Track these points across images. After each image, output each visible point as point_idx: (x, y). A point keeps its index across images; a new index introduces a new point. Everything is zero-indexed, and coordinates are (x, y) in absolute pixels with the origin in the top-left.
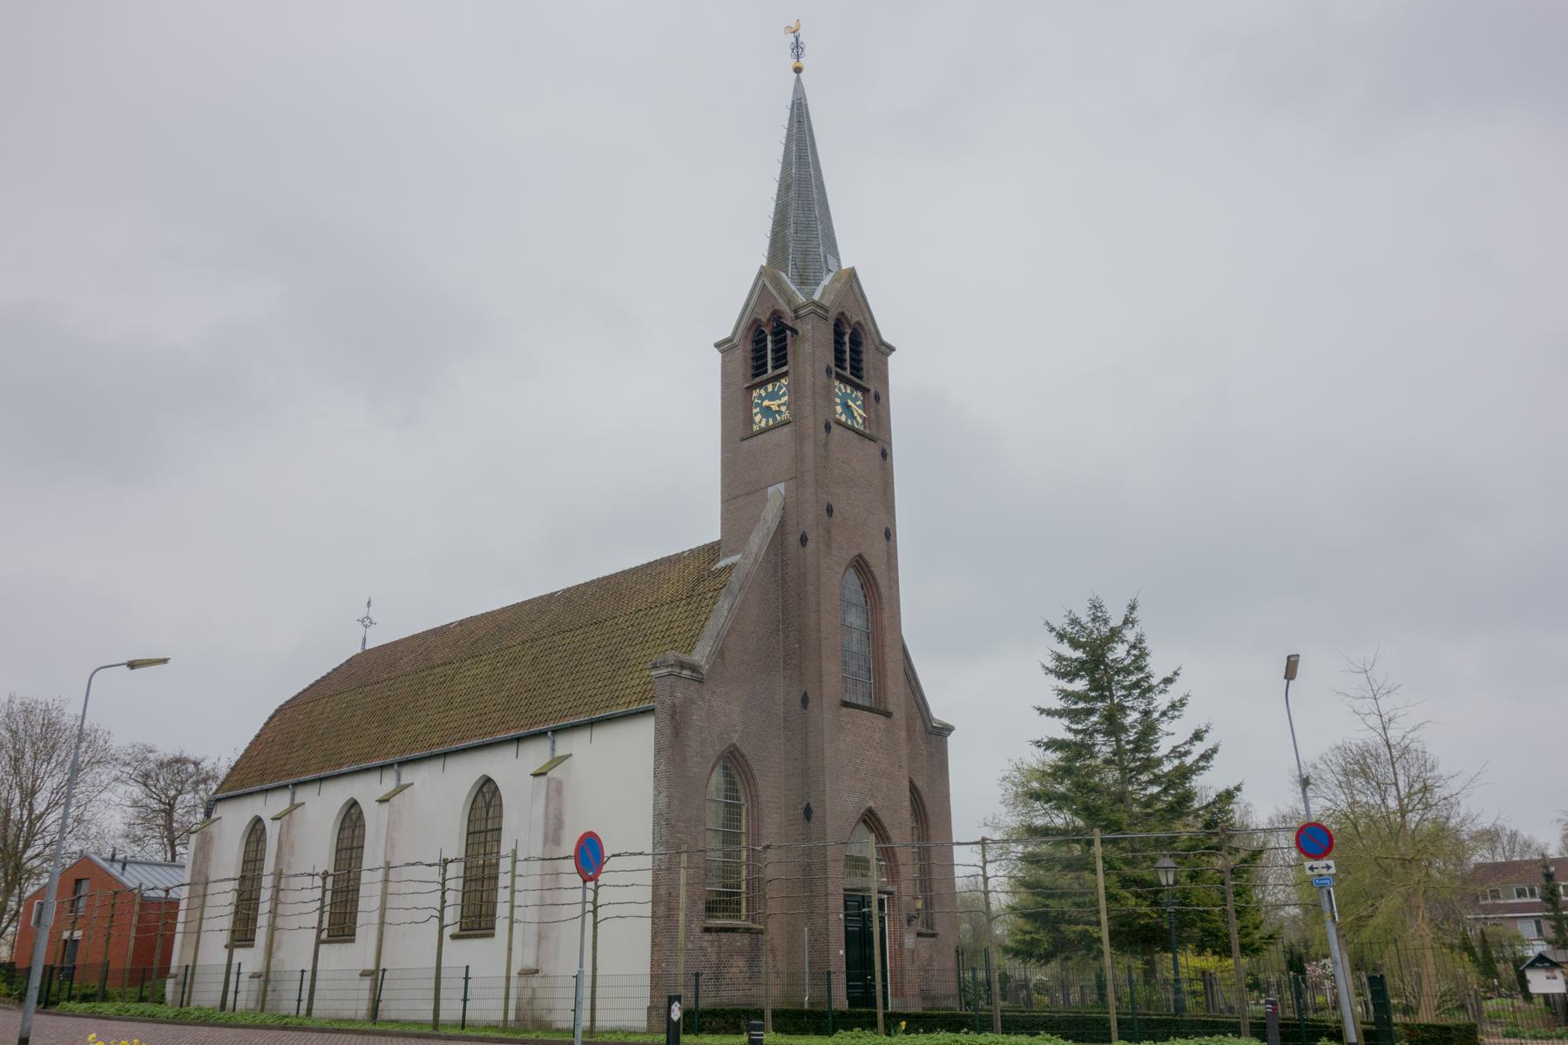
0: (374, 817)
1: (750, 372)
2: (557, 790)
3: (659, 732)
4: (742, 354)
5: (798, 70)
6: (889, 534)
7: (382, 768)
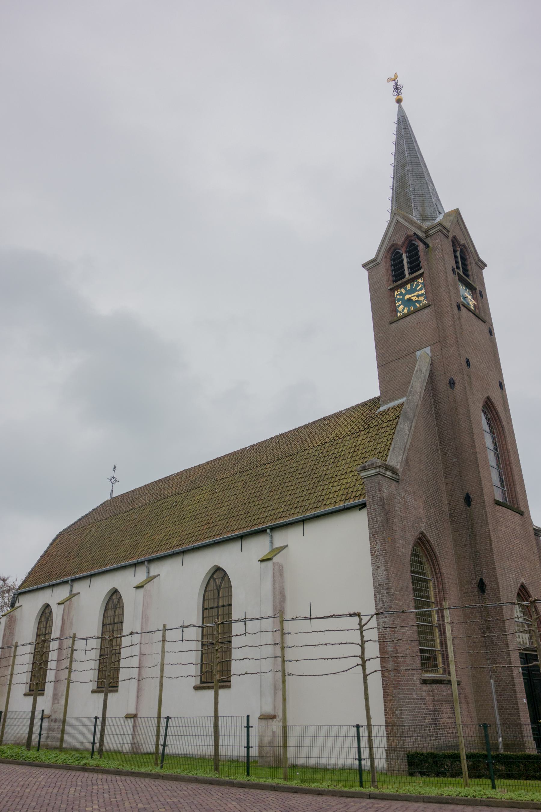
0: (131, 600)
1: (392, 279)
2: (279, 573)
3: (372, 521)
4: (384, 271)
5: (399, 101)
6: (501, 386)
7: (135, 565)
